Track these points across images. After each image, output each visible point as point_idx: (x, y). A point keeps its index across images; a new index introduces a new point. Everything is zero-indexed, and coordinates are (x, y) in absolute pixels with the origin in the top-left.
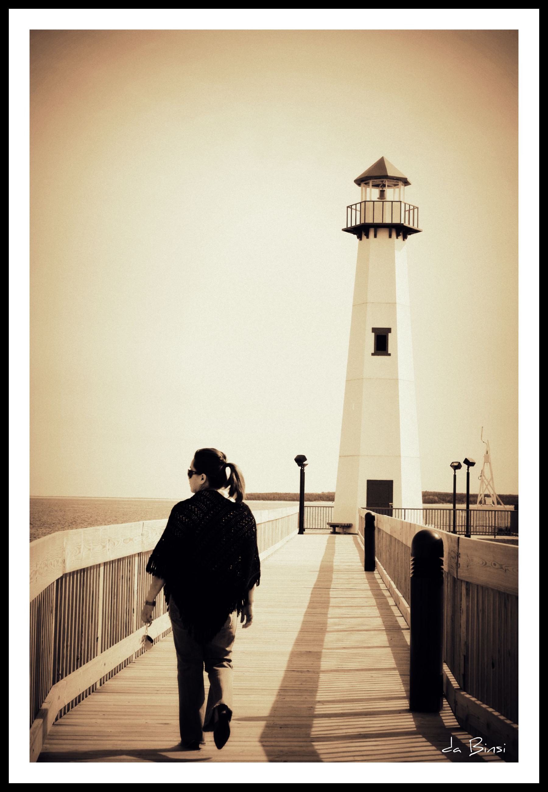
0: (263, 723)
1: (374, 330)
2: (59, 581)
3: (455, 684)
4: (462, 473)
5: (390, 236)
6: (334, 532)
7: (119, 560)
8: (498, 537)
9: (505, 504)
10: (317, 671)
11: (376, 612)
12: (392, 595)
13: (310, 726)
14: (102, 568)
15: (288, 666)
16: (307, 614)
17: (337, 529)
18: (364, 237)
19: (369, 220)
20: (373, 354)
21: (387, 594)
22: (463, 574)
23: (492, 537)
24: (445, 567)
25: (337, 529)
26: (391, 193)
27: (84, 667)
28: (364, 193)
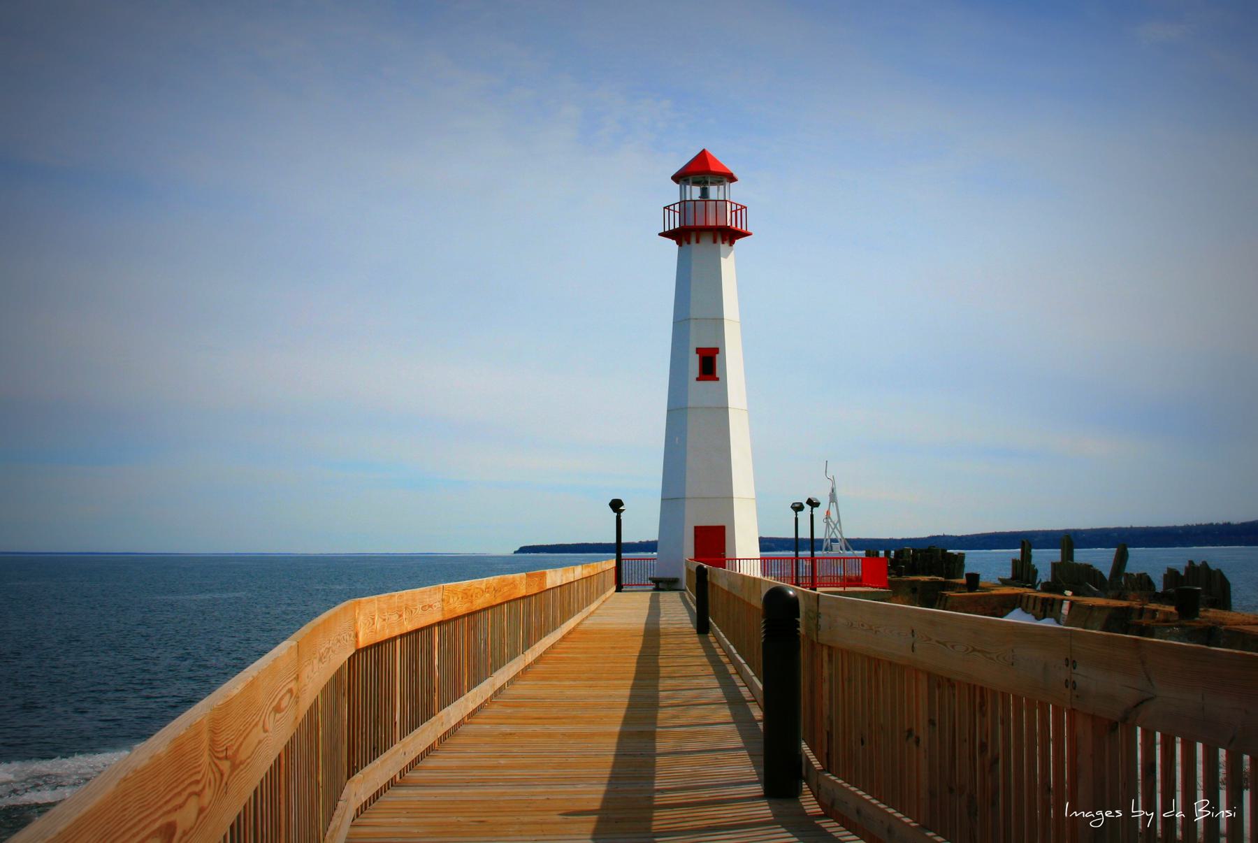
0: (594, 817)
1: (699, 350)
2: (351, 659)
3: (817, 764)
4: (804, 515)
5: (715, 242)
6: (657, 589)
7: (417, 631)
8: (848, 589)
9: (855, 549)
10: (653, 755)
11: (715, 682)
12: (733, 661)
13: (650, 820)
14: (398, 641)
15: (618, 750)
16: (633, 687)
17: (661, 585)
18: (685, 244)
19: (690, 223)
20: (698, 379)
21: (725, 660)
22: (824, 637)
23: (841, 589)
24: (801, 630)
25: (661, 585)
26: (714, 192)
27: (382, 757)
28: (683, 192)
